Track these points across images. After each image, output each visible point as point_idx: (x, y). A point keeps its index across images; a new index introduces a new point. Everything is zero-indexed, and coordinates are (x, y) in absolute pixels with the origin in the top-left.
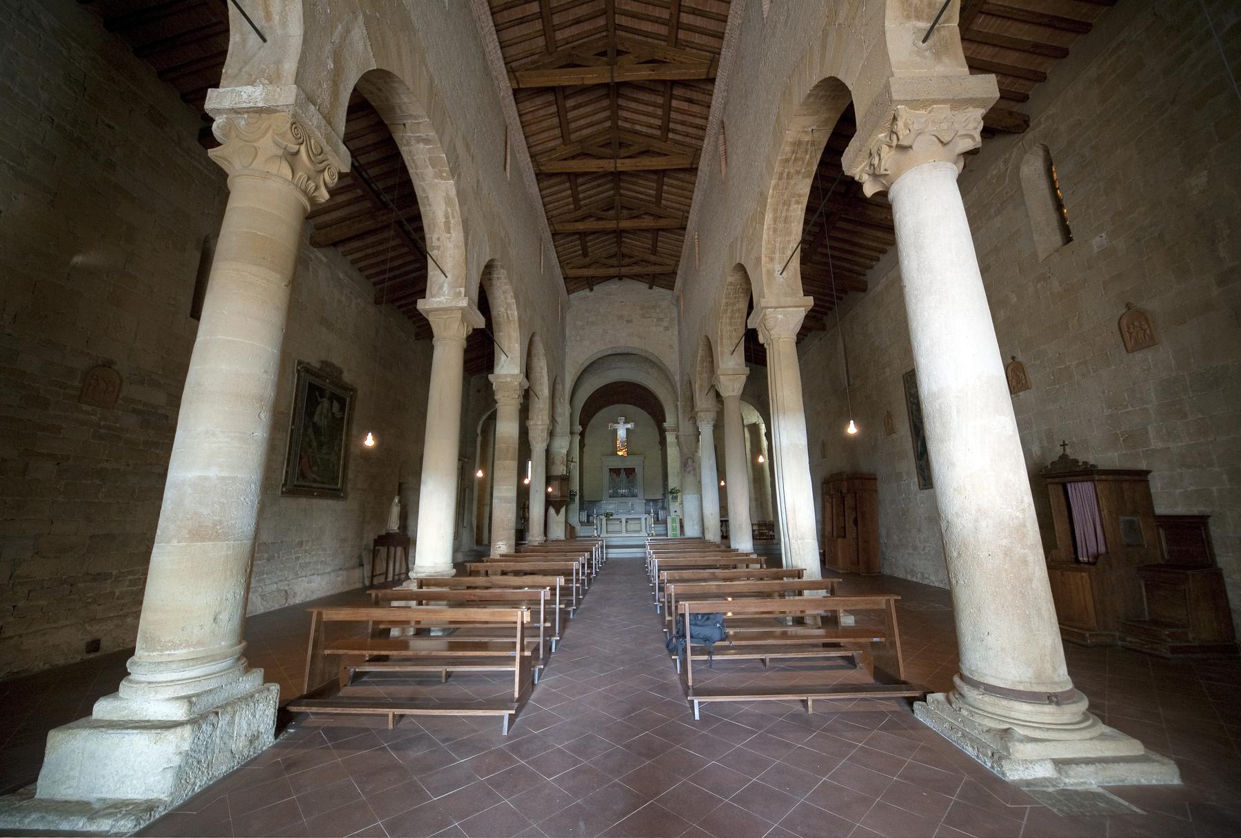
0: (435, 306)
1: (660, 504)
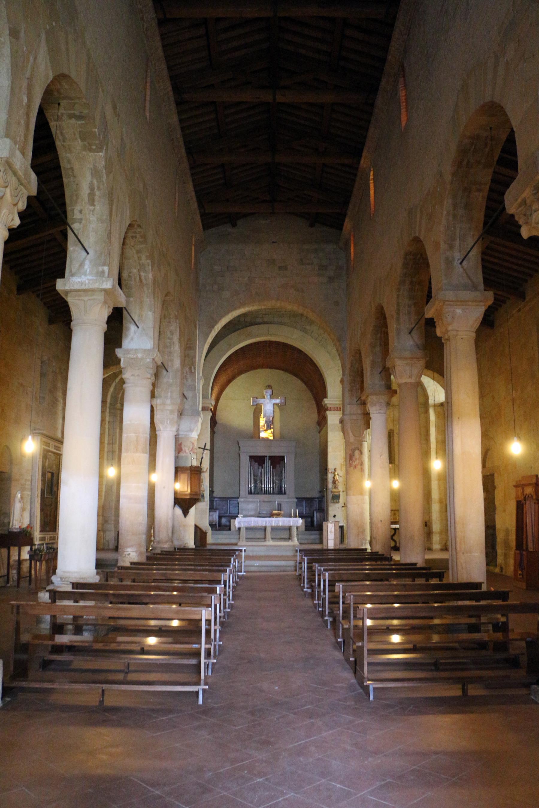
0: (76, 287)
1: (316, 505)
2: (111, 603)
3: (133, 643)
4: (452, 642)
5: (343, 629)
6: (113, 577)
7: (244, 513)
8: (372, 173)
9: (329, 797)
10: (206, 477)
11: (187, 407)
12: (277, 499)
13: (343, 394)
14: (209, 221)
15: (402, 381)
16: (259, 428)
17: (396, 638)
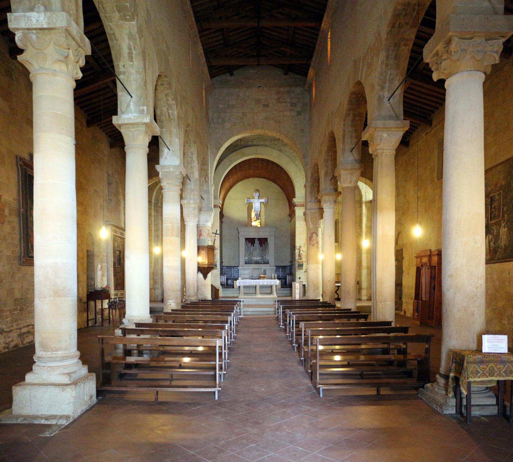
0: (126, 122)
1: (288, 271)
2: (160, 336)
3: (174, 361)
4: (372, 361)
5: (304, 352)
6: (161, 319)
7: (243, 276)
8: (329, 33)
9: (295, 455)
10: (217, 252)
11: (204, 205)
12: (263, 267)
13: (306, 194)
14: (214, 71)
15: (345, 185)
16: (251, 219)
17: (337, 358)
